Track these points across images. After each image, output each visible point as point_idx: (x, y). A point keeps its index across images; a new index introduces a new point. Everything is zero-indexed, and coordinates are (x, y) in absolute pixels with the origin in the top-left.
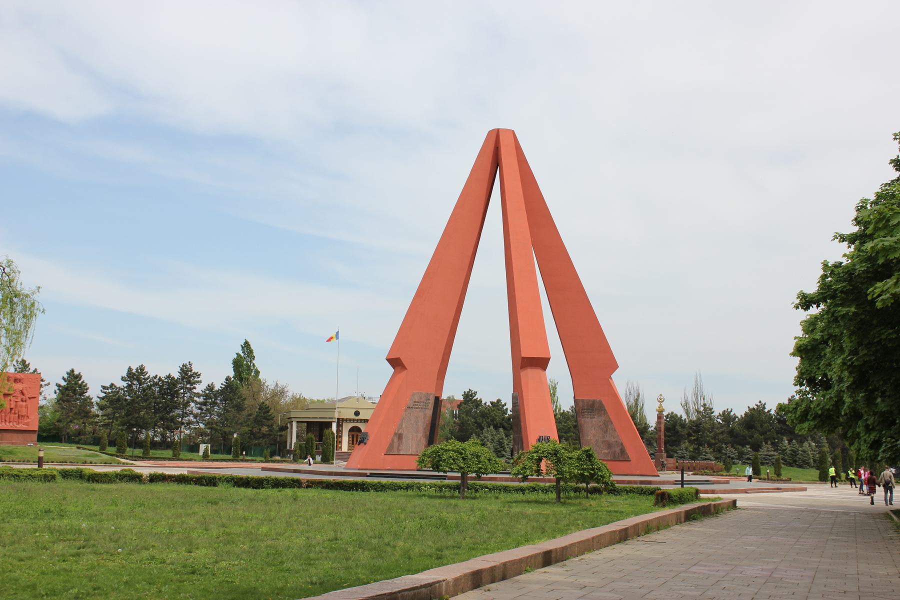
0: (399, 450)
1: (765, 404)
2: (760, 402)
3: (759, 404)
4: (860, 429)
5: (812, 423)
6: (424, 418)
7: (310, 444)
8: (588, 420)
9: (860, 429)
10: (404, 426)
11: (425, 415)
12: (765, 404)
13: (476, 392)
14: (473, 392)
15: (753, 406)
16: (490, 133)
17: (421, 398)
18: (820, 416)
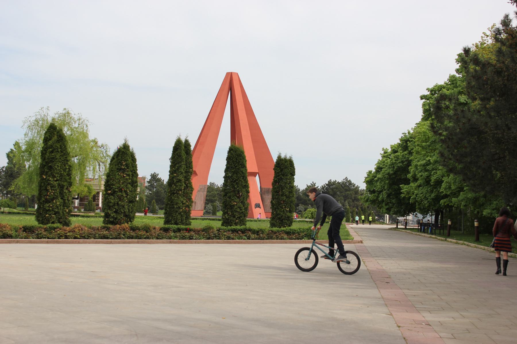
0: (195, 208)
1: (315, 183)
2: (313, 182)
3: (312, 183)
4: (384, 205)
5: (369, 203)
6: (204, 195)
7: (91, 203)
8: (267, 196)
9: (384, 205)
10: (197, 198)
11: (204, 194)
12: (315, 183)
13: (158, 174)
14: (156, 174)
15: (309, 184)
16: (228, 74)
17: (202, 187)
18: (372, 201)
